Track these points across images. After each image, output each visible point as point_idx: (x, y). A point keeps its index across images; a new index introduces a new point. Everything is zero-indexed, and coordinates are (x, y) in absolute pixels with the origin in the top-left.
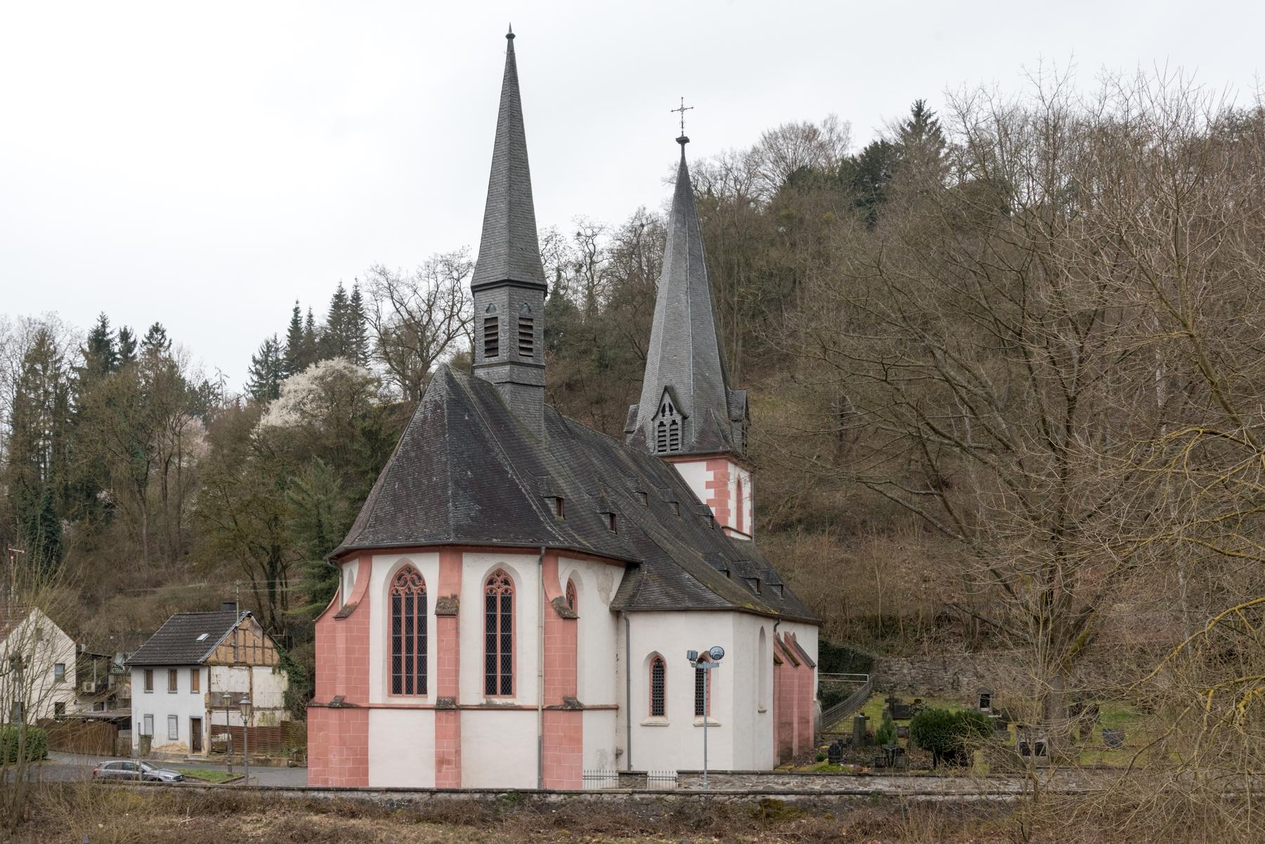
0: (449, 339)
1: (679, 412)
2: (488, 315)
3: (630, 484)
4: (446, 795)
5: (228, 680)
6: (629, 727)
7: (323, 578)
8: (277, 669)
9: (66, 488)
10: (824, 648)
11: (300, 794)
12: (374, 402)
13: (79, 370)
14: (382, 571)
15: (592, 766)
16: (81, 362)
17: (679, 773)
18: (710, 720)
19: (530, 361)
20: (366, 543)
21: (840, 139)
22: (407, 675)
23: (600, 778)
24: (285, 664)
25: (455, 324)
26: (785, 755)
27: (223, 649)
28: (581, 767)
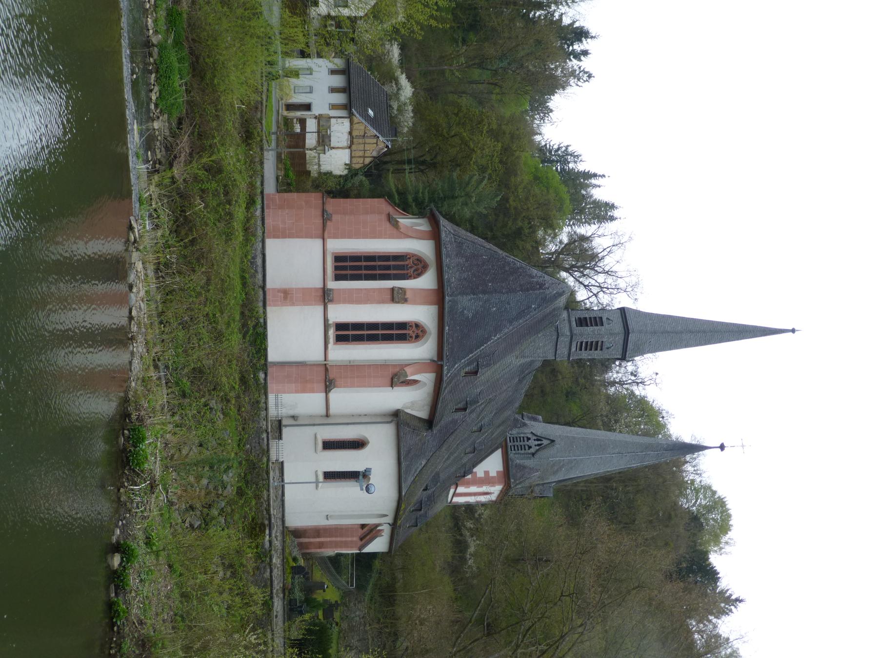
0: (585, 286)
1: (538, 450)
2: (604, 319)
3: (487, 419)
4: (261, 297)
5: (340, 130)
6: (314, 425)
7: (415, 199)
8: (349, 167)
9: (475, 8)
10: (373, 555)
11: (259, 191)
12: (540, 233)
13: (560, 19)
14: (423, 248)
15: (284, 401)
16: (566, 21)
17: (282, 463)
18: (320, 485)
19: (573, 349)
20: (443, 235)
21: (721, 549)
22: (349, 267)
23: (277, 405)
24: (352, 172)
25: (595, 290)
26: (298, 533)
27: (363, 128)
28: (284, 392)
